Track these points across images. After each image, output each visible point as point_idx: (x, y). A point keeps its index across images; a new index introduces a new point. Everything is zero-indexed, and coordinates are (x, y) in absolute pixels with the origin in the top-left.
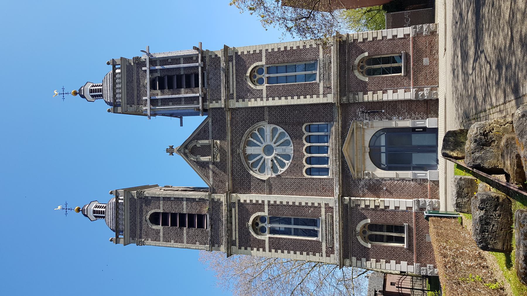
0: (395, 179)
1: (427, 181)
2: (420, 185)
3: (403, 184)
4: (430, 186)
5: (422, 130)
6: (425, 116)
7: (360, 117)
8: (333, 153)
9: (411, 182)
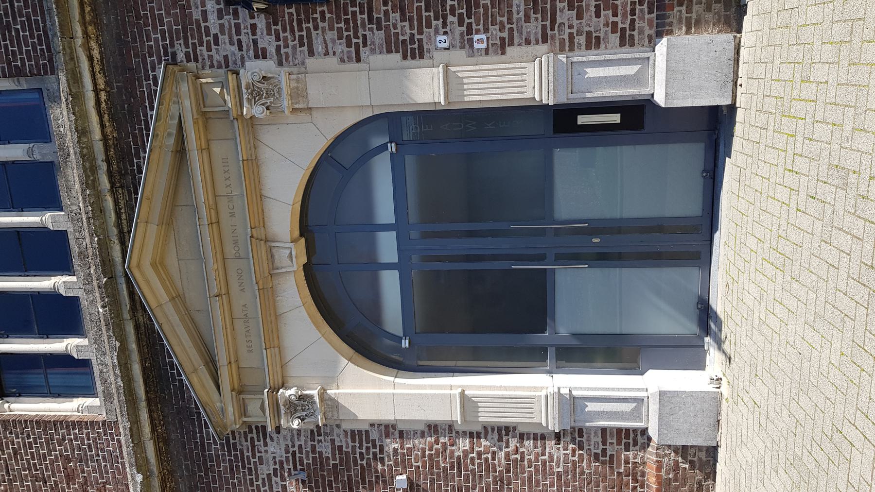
0: (457, 428)
1: (640, 440)
2: (603, 463)
3: (502, 454)
4: (659, 469)
5: (616, 118)
6: (645, 24)
7: (216, 37)
8: (90, 275)
9: (548, 443)
